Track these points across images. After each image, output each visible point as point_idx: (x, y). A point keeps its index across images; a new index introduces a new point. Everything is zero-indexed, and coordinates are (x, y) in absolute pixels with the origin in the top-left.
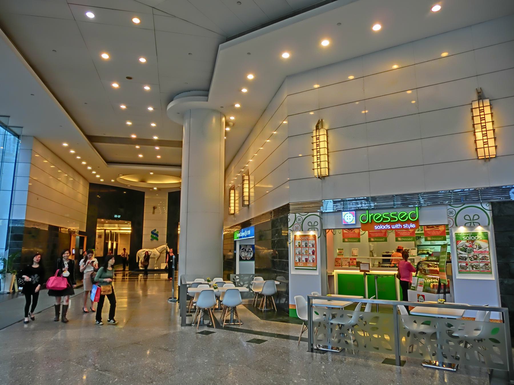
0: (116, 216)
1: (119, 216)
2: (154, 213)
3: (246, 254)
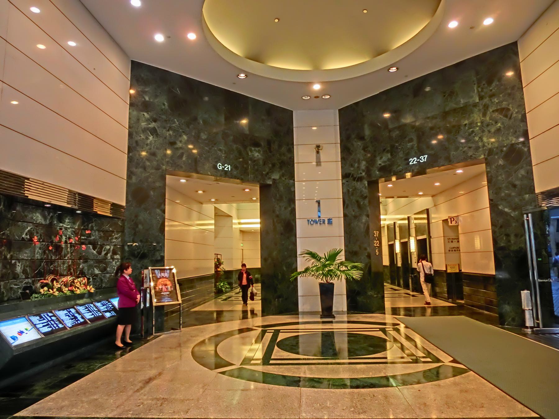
2: (319, 163)
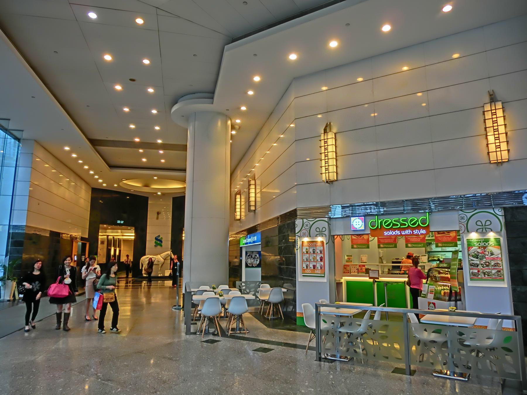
0: (119, 222)
1: (122, 222)
2: (157, 218)
3: (252, 261)
